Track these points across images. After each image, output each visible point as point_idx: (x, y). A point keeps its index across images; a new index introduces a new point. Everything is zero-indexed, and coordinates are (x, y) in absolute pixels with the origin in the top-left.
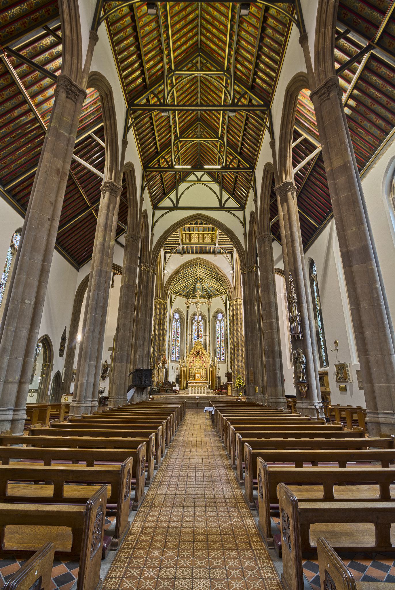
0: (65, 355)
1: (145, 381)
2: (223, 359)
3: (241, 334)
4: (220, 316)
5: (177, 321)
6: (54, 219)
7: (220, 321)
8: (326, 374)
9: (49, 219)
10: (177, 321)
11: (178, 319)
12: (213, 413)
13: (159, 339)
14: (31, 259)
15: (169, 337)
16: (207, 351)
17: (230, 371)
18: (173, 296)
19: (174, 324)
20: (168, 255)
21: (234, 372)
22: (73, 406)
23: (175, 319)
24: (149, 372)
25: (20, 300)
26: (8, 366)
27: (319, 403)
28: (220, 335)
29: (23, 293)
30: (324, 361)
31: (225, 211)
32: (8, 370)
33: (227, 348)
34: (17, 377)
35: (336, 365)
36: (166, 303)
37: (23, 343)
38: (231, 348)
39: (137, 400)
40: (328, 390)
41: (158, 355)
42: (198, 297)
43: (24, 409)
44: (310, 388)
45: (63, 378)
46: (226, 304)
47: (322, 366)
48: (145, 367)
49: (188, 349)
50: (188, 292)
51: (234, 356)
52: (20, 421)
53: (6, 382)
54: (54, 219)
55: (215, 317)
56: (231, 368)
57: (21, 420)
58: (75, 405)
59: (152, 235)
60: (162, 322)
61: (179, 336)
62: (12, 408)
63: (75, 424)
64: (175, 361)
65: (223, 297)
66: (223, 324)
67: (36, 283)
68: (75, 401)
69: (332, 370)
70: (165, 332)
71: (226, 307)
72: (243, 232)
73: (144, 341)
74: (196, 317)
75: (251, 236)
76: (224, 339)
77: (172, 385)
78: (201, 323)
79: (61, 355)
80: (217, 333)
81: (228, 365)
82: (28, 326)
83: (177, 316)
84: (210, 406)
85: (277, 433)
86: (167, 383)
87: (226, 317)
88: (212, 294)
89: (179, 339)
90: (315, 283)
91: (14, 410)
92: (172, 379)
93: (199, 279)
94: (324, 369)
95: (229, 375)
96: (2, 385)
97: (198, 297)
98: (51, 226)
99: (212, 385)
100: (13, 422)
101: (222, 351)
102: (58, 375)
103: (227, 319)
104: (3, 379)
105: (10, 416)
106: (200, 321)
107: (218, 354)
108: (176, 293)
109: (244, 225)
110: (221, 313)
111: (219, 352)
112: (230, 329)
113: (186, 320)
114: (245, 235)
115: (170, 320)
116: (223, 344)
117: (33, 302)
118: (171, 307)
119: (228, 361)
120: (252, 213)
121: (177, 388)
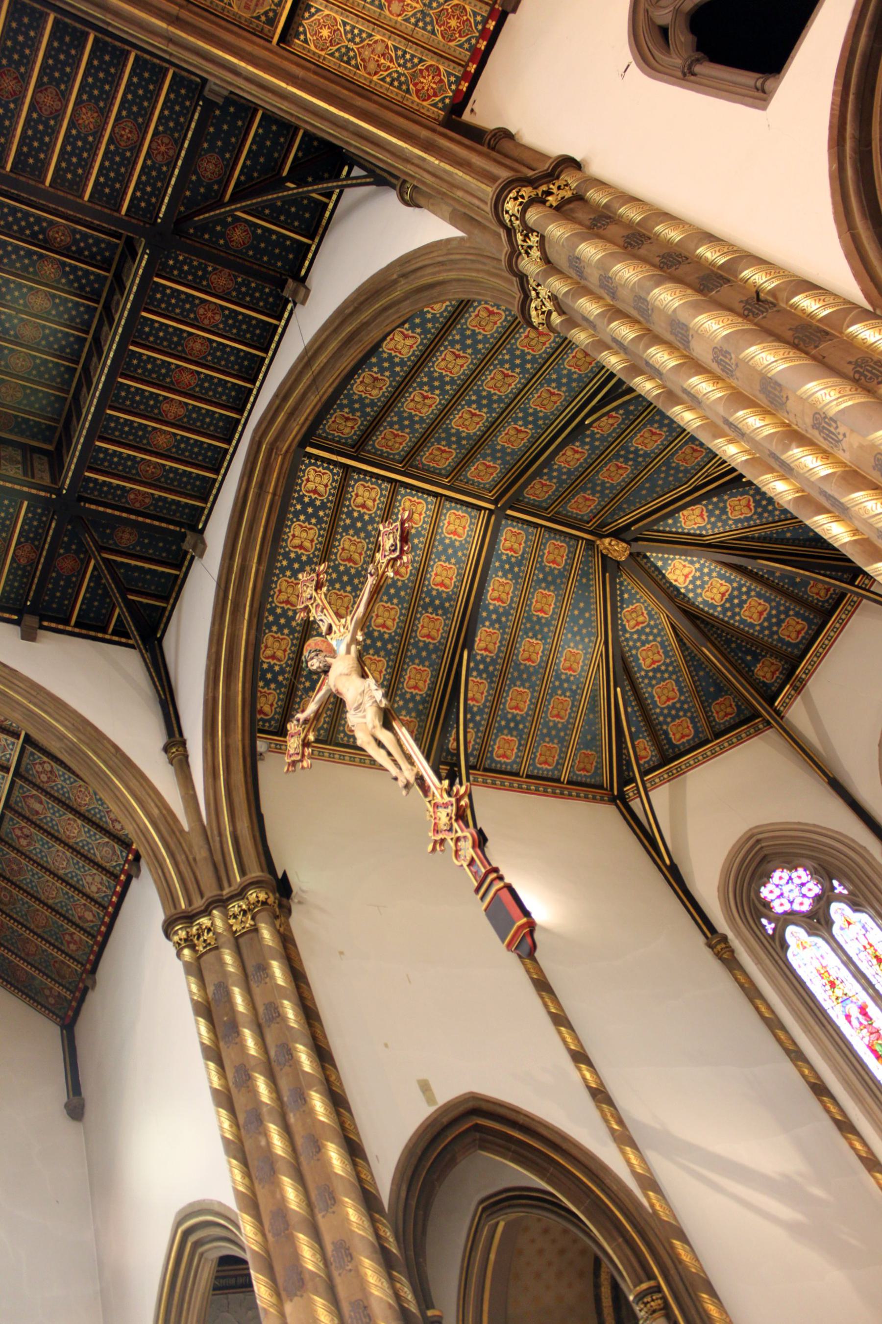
23: (790, 918)
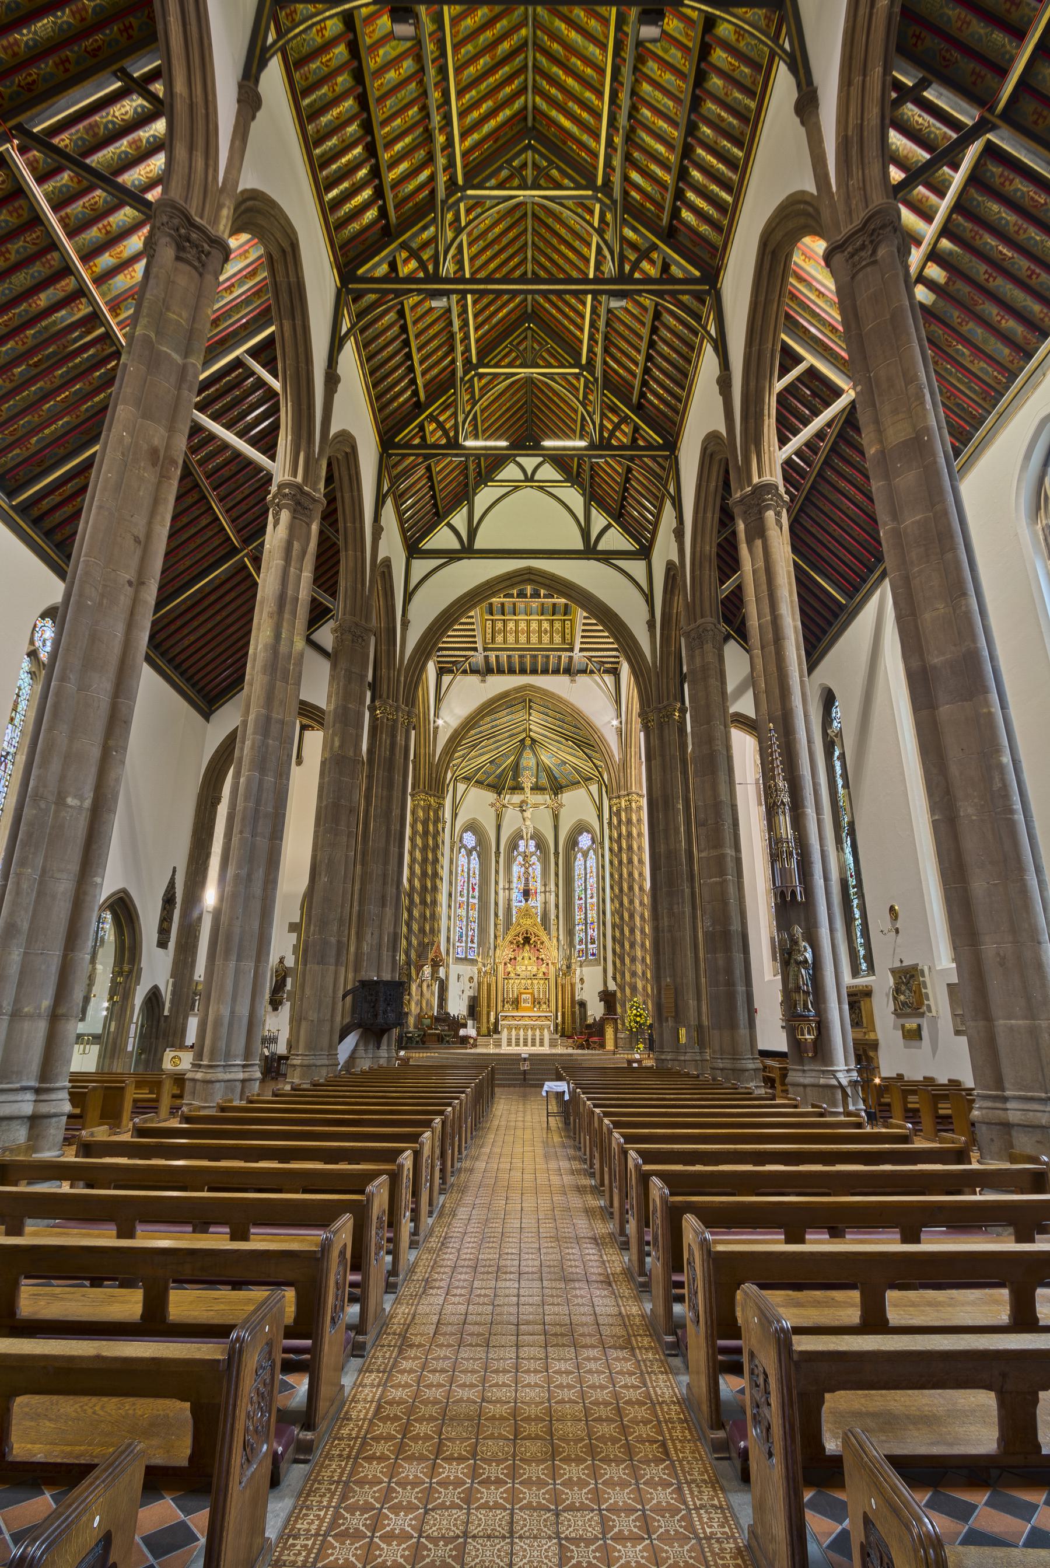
0: (172, 945)
1: (385, 1012)
2: (593, 954)
3: (641, 889)
4: (585, 841)
5: (469, 853)
6: (143, 583)
7: (585, 855)
9: (130, 583)
10: (469, 853)
11: (474, 848)
12: (567, 1097)
13: (423, 902)
15: (450, 895)
16: (549, 934)
17: (612, 986)
18: (461, 787)
19: (463, 860)
20: (446, 679)
21: (622, 988)
22: (194, 1080)
23: (465, 847)
24: (397, 990)
26: (22, 973)
27: (848, 1071)
28: (586, 889)
29: (62, 778)
30: (862, 960)
31: (598, 560)
32: (20, 984)
33: (604, 924)
34: (46, 1003)
35: (893, 971)
36: (441, 806)
38: (614, 926)
39: (364, 1064)
40: (872, 1036)
41: (419, 944)
42: (528, 790)
43: (63, 1088)
44: (823, 1031)
45: (167, 1005)
46: (600, 809)
47: (855, 972)
48: (387, 976)
49: (501, 928)
50: (499, 777)
51: (622, 946)
52: (54, 1120)
53: (16, 1015)
54: (143, 583)
55: (572, 843)
56: (614, 978)
57: (55, 1115)
58: (199, 1076)
59: (405, 624)
60: (430, 856)
61: (476, 893)
62: (33, 1083)
63: (200, 1126)
64: (466, 959)
65: (594, 788)
66: (592, 862)
67: (96, 752)
69: (882, 983)
70: (438, 881)
71: (600, 817)
72: (646, 616)
75: (667, 626)
76: (595, 900)
77: (456, 1024)
78: (534, 859)
79: (162, 944)
80: (578, 884)
81: (605, 971)
82: (74, 867)
83: (470, 840)
84: (560, 1078)
85: (736, 1152)
87: (602, 843)
88: (564, 782)
89: (476, 901)
90: (837, 753)
91: (38, 1091)
92: (457, 1007)
93: (528, 742)
94: (860, 981)
95: (608, 998)
96: (5, 1024)
97: (528, 790)
98: (135, 601)
99: (563, 1022)
100: (35, 1121)
101: (590, 932)
102: (154, 997)
103: (603, 848)
105: (26, 1105)
106: (532, 854)
107: (581, 941)
108: (467, 779)
109: (649, 599)
110: (588, 832)
111: (583, 935)
112: (612, 875)
113: (494, 849)
114: (651, 624)
115: (452, 850)
116: (592, 915)
117: (88, 803)
118: (454, 815)
119: (605, 959)
120: (670, 566)
121: (470, 1031)
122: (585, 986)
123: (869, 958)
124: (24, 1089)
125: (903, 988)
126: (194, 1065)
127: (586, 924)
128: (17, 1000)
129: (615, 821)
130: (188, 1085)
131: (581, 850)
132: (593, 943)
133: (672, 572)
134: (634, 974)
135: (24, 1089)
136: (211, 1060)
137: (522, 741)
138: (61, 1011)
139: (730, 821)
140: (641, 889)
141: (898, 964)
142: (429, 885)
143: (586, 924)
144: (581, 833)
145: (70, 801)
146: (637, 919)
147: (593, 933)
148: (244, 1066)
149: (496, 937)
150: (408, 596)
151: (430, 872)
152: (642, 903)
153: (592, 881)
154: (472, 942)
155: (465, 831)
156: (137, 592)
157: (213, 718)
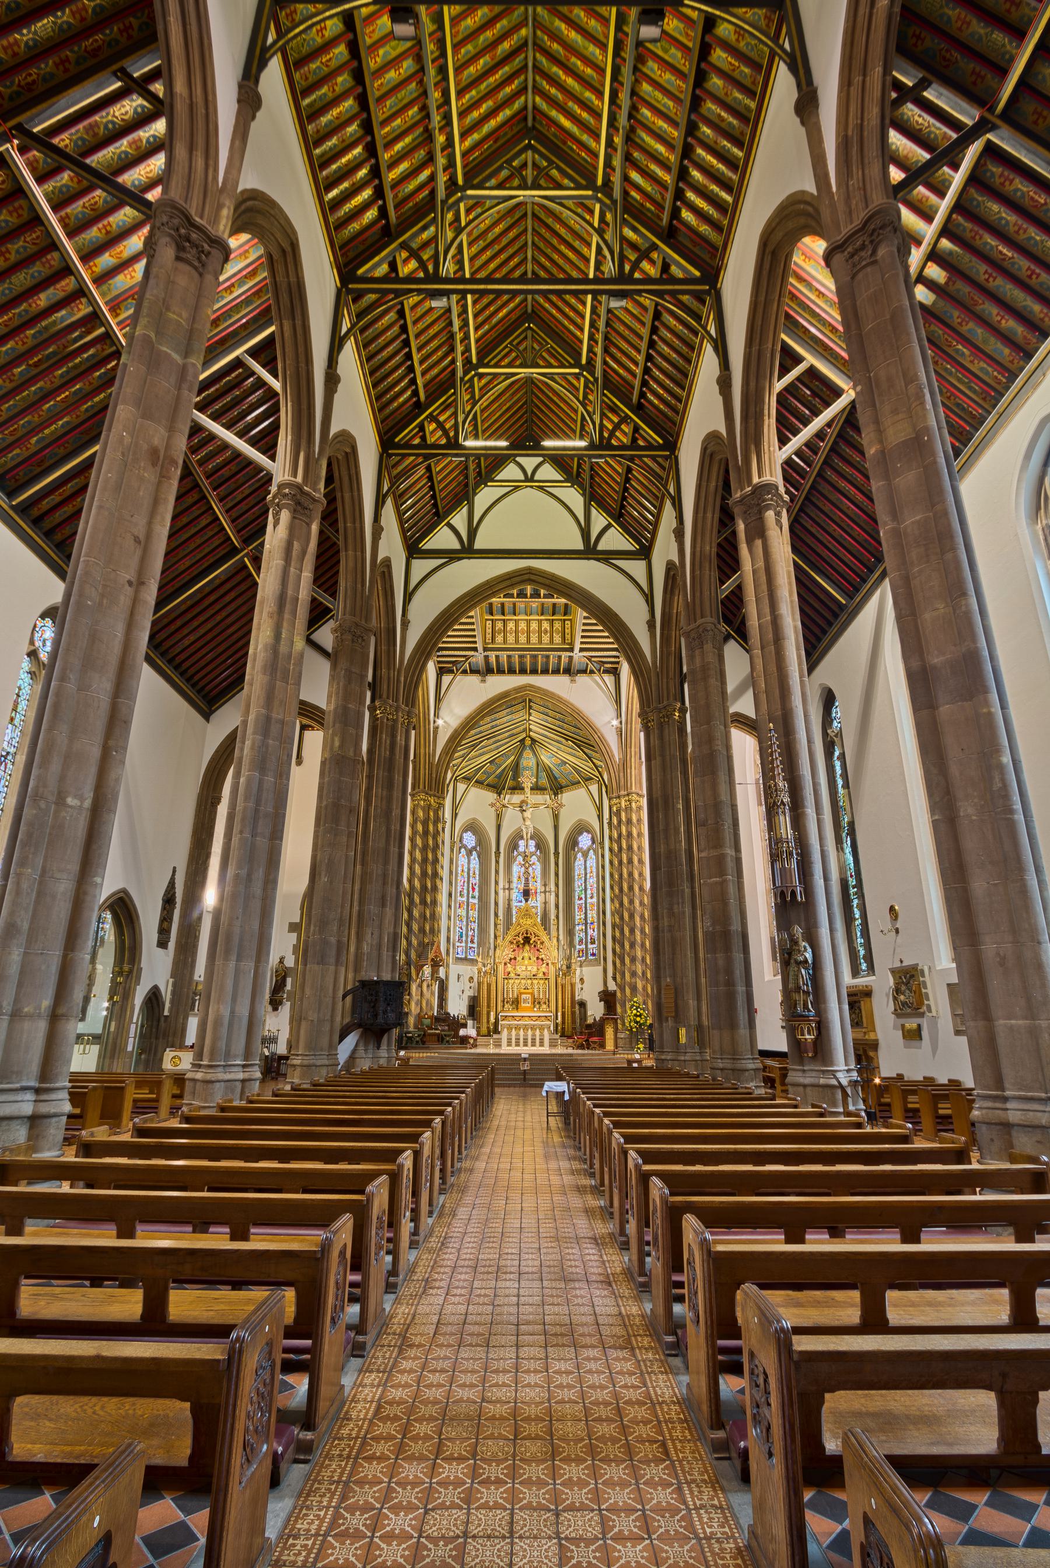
0: (172, 945)
1: (385, 1012)
2: (593, 954)
3: (641, 889)
4: (585, 841)
5: (469, 853)
6: (143, 583)
7: (585, 855)
8: (868, 993)
9: (130, 583)
10: (469, 853)
11: (474, 848)
12: (567, 1097)
13: (423, 902)
14: (83, 687)
16: (549, 934)
17: (612, 986)
18: (461, 787)
19: (462, 860)
21: (622, 989)
22: (194, 1080)
23: (465, 847)
24: (396, 990)
25: (52, 798)
26: (22, 972)
28: (586, 890)
29: (62, 778)
30: (862, 960)
31: (598, 560)
32: (20, 985)
33: (604, 924)
34: (46, 1003)
35: (893, 971)
36: (441, 806)
37: (61, 911)
38: (614, 926)
39: (364, 1064)
40: (872, 1036)
42: (528, 790)
44: (823, 1031)
45: (167, 1005)
46: (600, 809)
47: (855, 972)
48: (386, 976)
51: (622, 946)
52: (54, 1120)
53: (16, 1015)
54: (143, 583)
55: (572, 843)
56: (614, 978)
58: (199, 1076)
59: (405, 624)
60: (430, 856)
61: (476, 893)
62: (33, 1083)
63: (200, 1127)
64: (466, 959)
65: (594, 788)
66: (592, 861)
67: (96, 752)
68: (200, 1066)
70: (438, 881)
71: (600, 817)
72: (646, 616)
73: (383, 905)
74: (522, 843)
75: (667, 626)
76: (595, 900)
77: (456, 1024)
78: (534, 859)
79: (162, 944)
80: (578, 884)
81: (605, 971)
82: (74, 867)
83: (470, 840)
84: (560, 1078)
86: (444, 1018)
88: (564, 782)
89: (476, 901)
91: (37, 1091)
92: (457, 1007)
93: (528, 742)
94: (862, 981)
95: (608, 998)
96: (5, 1024)
97: (528, 790)
101: (590, 932)
102: (154, 997)
103: (603, 848)
104: (7, 1007)
106: (532, 854)
107: (581, 941)
108: (468, 779)
109: (649, 599)
110: (588, 832)
111: (583, 935)
112: (612, 875)
113: (494, 849)
114: (651, 624)
116: (592, 915)
117: (88, 803)
118: (454, 815)
119: (605, 959)
120: (670, 567)
121: (470, 1031)
122: (585, 986)
123: (869, 958)
124: (24, 1089)
125: (903, 988)
126: (194, 1065)
127: (586, 924)
128: (16, 1000)
129: (615, 821)
130: (188, 1085)
131: (581, 850)
132: (593, 943)
133: (672, 572)
134: (634, 974)
135: (24, 1089)
136: (210, 1060)
137: (522, 741)
138: (61, 1011)
139: (730, 821)
140: (641, 889)
141: (898, 964)
142: (429, 885)
143: (586, 924)
144: (581, 833)
145: (70, 801)
146: (637, 919)
147: (592, 933)
148: (244, 1066)
149: (496, 937)
150: (408, 596)
151: (430, 872)
152: (642, 903)
153: (592, 881)
154: (472, 942)
155: (465, 830)
156: (137, 592)
157: (214, 717)
